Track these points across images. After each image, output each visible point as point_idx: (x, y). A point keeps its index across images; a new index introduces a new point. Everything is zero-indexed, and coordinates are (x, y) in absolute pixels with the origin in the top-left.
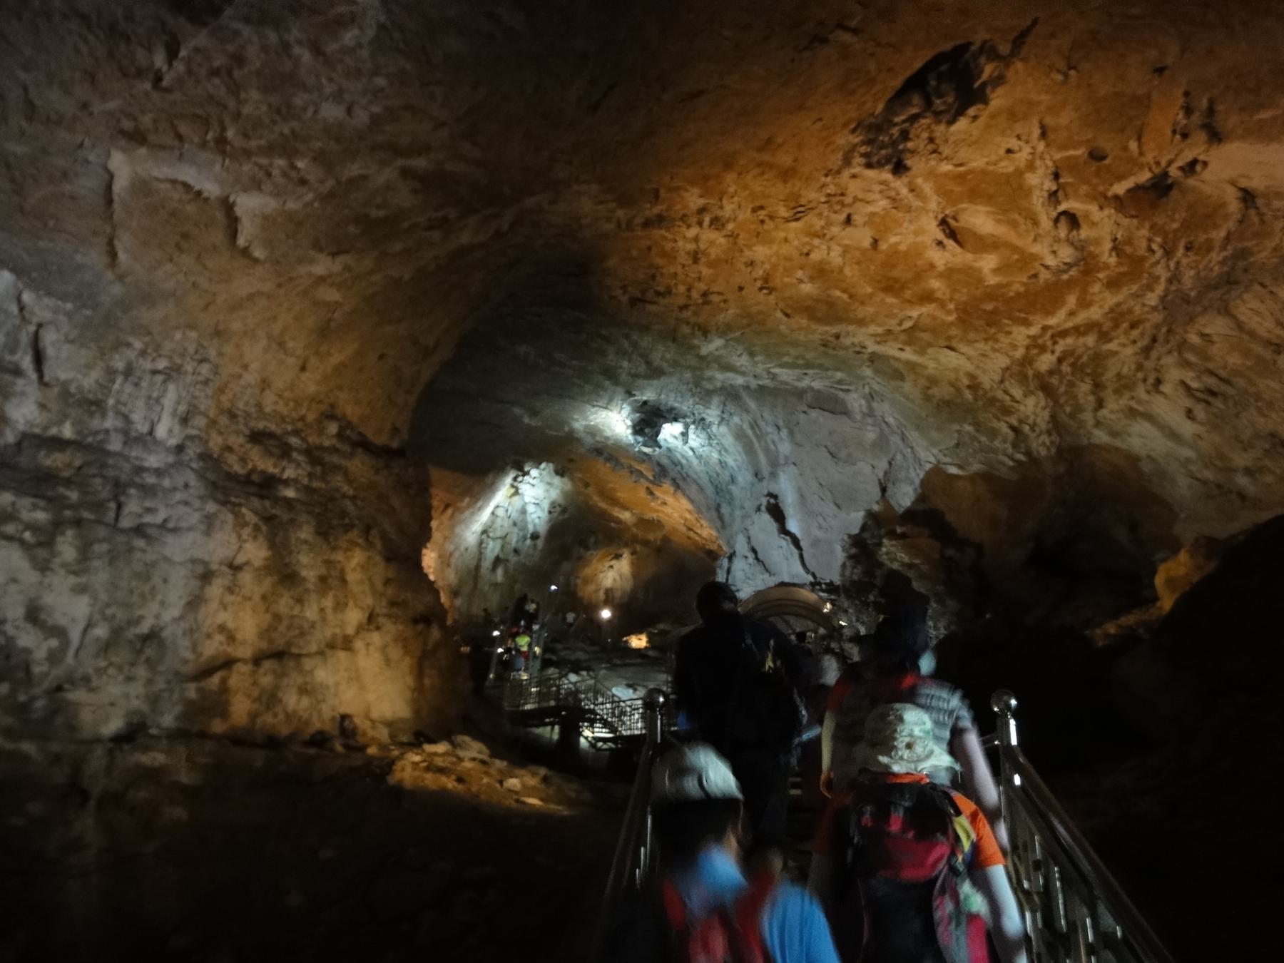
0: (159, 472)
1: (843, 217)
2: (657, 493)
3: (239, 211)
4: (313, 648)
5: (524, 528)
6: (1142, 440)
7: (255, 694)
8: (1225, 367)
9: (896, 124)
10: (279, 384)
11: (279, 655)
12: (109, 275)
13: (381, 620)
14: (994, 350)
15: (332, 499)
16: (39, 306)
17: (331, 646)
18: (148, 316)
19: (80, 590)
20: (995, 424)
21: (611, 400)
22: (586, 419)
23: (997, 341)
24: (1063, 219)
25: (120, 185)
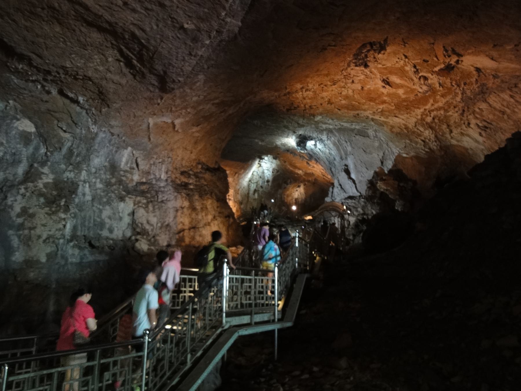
0: (164, 187)
1: (351, 81)
2: (310, 163)
3: (176, 123)
4: (201, 225)
5: (264, 178)
6: (467, 143)
7: (190, 237)
8: (489, 119)
9: (363, 53)
10: (186, 158)
11: (194, 228)
12: (149, 143)
13: (217, 217)
14: (411, 116)
15: (202, 187)
16: (137, 153)
17: (205, 225)
18: (157, 150)
19: (155, 216)
20: (416, 140)
21: (288, 135)
22: (281, 141)
23: (411, 114)
24: (422, 78)
25: (151, 125)
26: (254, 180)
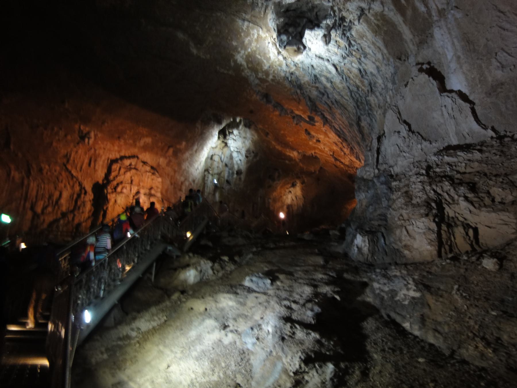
2: (313, 133)
5: (232, 168)
26: (213, 169)
